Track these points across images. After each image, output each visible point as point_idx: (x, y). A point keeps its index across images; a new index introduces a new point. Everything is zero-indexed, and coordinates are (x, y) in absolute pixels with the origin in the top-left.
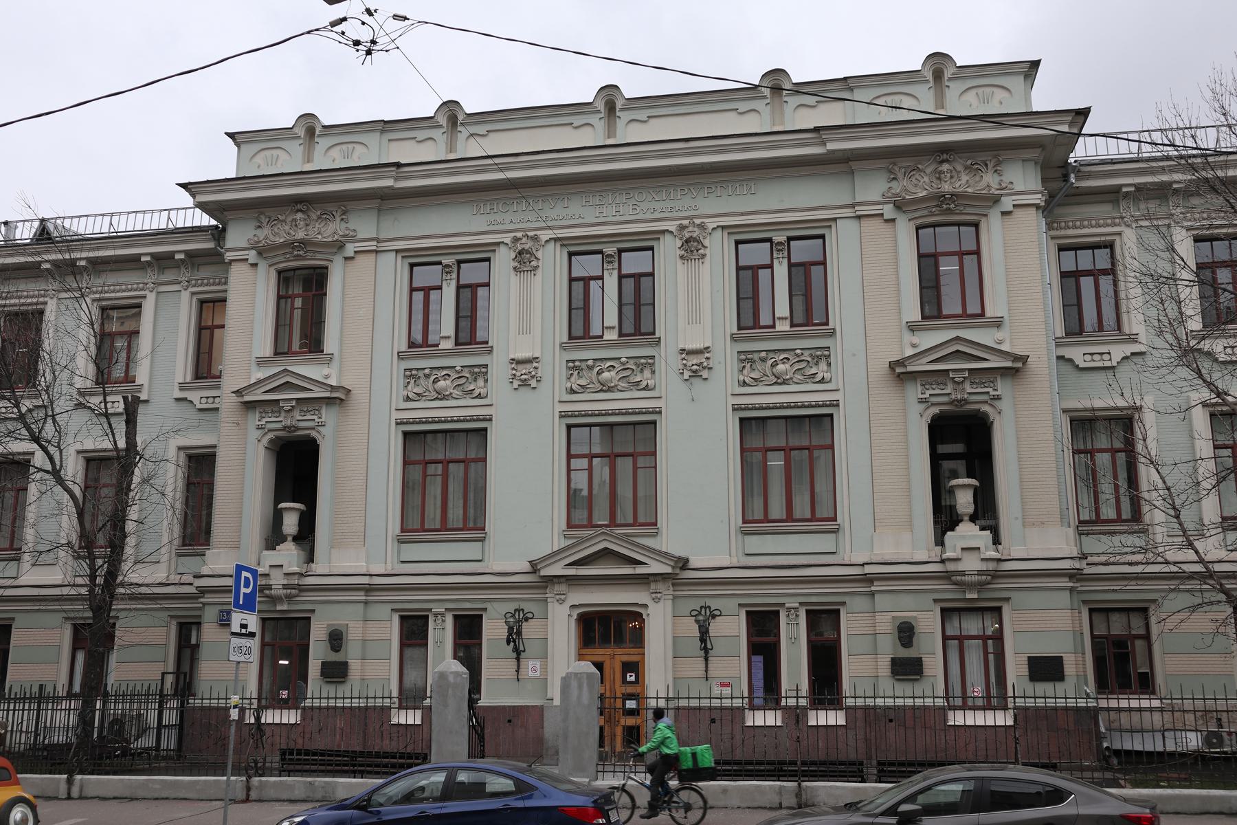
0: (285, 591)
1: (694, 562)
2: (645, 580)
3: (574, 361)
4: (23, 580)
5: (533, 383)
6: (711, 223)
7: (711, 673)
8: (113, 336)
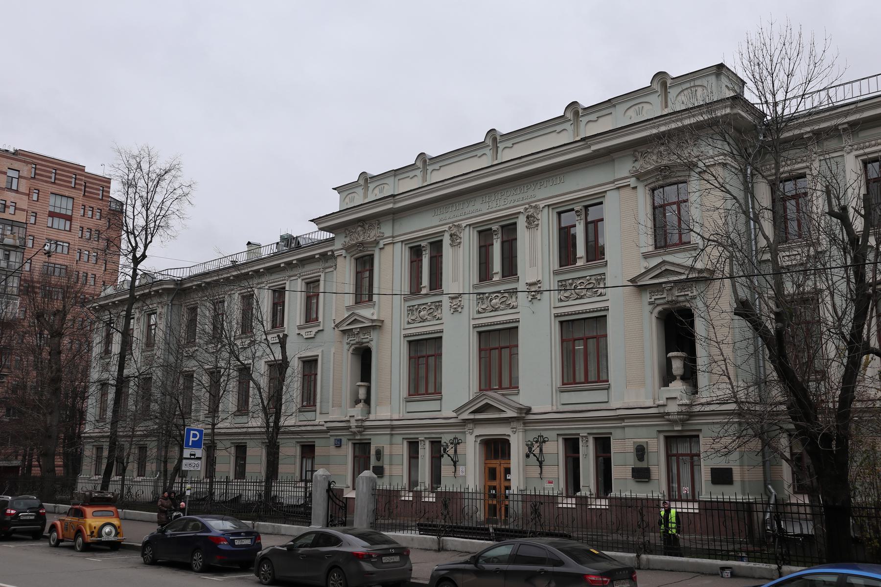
0: (679, 416)
1: (534, 410)
2: (507, 421)
3: (410, 307)
4: (250, 425)
5: (460, 310)
6: (542, 204)
7: (545, 474)
8: (785, 199)
